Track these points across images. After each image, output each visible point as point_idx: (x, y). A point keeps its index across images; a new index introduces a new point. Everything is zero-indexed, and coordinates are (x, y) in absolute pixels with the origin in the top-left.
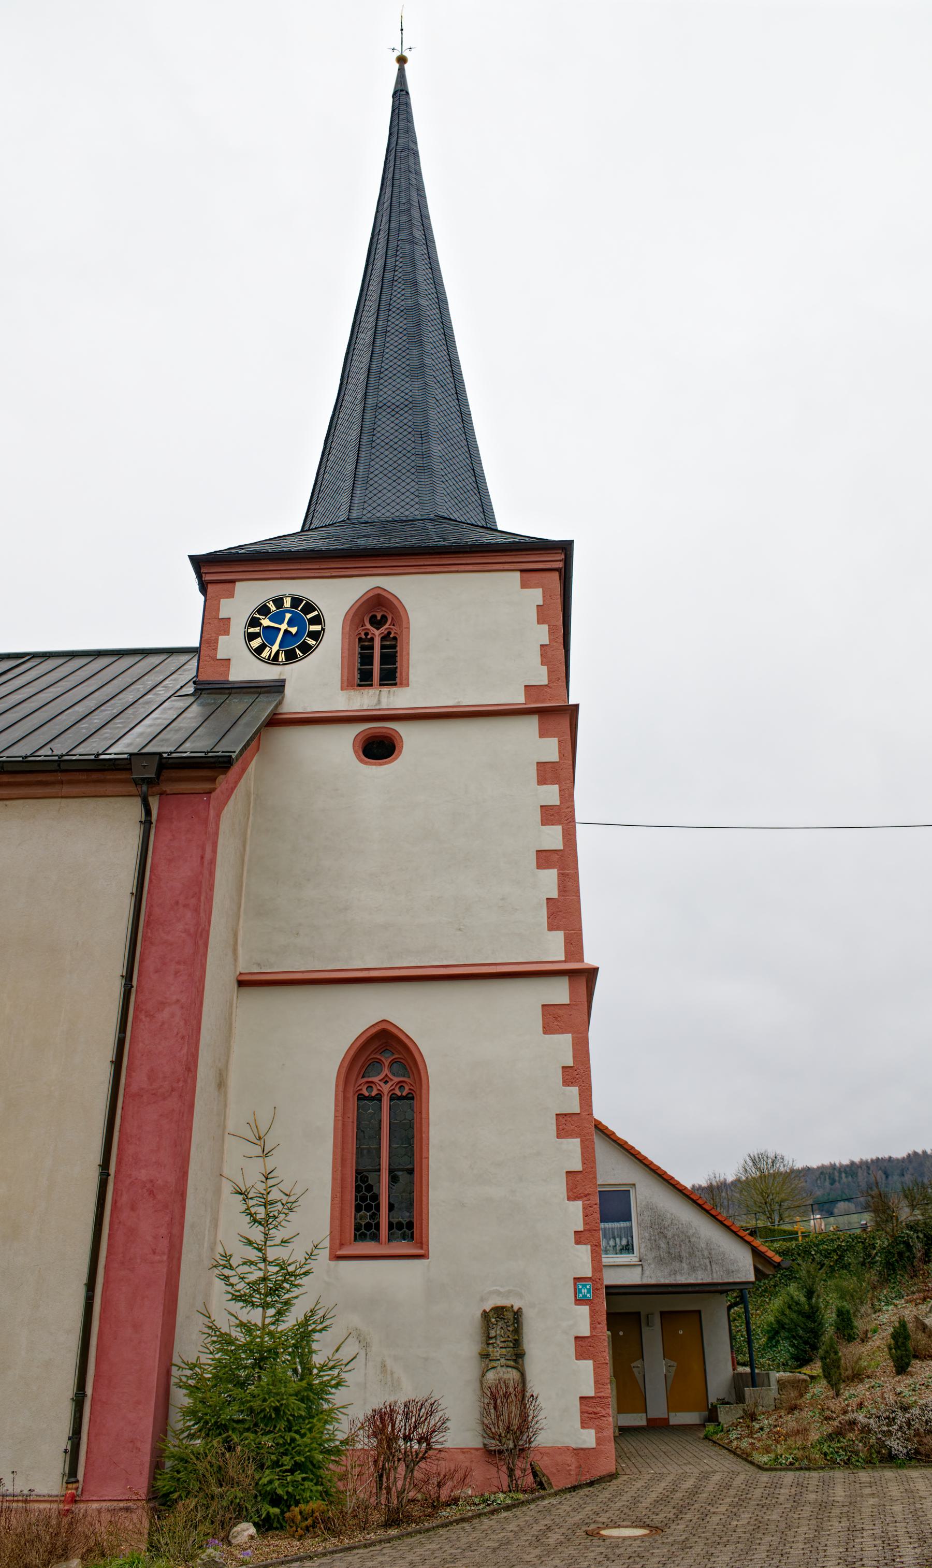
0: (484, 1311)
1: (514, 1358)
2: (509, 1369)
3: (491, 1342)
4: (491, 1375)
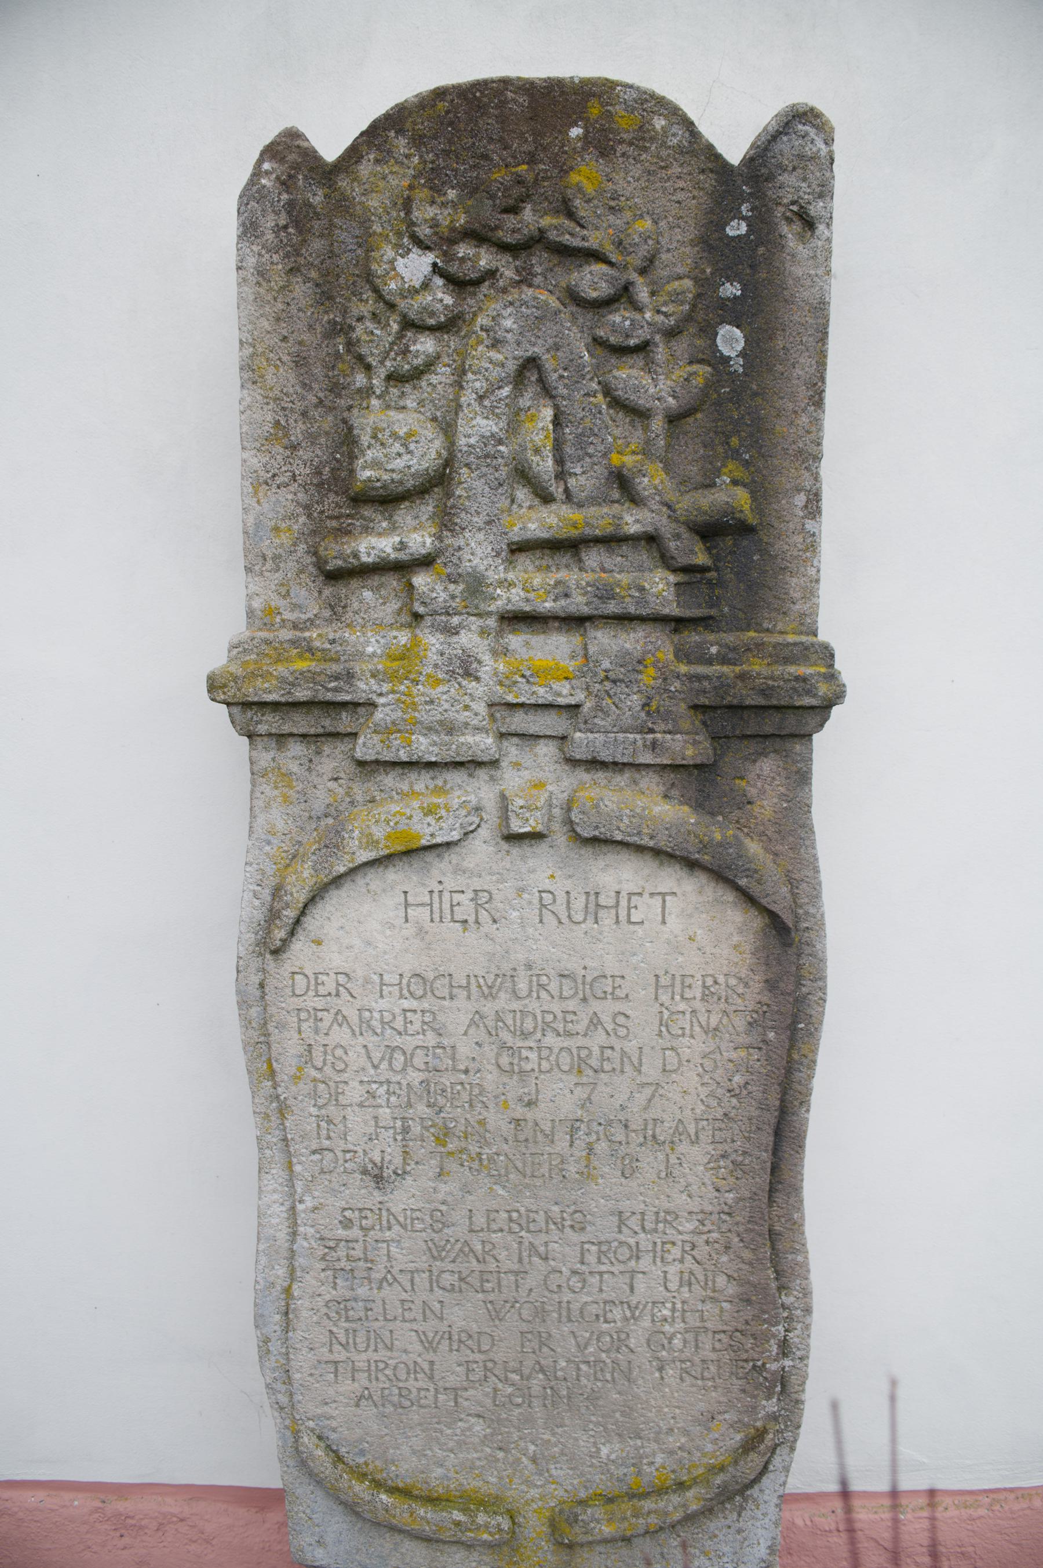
0: (288, 153)
1: (686, 746)
2: (619, 875)
3: (376, 545)
4: (367, 931)
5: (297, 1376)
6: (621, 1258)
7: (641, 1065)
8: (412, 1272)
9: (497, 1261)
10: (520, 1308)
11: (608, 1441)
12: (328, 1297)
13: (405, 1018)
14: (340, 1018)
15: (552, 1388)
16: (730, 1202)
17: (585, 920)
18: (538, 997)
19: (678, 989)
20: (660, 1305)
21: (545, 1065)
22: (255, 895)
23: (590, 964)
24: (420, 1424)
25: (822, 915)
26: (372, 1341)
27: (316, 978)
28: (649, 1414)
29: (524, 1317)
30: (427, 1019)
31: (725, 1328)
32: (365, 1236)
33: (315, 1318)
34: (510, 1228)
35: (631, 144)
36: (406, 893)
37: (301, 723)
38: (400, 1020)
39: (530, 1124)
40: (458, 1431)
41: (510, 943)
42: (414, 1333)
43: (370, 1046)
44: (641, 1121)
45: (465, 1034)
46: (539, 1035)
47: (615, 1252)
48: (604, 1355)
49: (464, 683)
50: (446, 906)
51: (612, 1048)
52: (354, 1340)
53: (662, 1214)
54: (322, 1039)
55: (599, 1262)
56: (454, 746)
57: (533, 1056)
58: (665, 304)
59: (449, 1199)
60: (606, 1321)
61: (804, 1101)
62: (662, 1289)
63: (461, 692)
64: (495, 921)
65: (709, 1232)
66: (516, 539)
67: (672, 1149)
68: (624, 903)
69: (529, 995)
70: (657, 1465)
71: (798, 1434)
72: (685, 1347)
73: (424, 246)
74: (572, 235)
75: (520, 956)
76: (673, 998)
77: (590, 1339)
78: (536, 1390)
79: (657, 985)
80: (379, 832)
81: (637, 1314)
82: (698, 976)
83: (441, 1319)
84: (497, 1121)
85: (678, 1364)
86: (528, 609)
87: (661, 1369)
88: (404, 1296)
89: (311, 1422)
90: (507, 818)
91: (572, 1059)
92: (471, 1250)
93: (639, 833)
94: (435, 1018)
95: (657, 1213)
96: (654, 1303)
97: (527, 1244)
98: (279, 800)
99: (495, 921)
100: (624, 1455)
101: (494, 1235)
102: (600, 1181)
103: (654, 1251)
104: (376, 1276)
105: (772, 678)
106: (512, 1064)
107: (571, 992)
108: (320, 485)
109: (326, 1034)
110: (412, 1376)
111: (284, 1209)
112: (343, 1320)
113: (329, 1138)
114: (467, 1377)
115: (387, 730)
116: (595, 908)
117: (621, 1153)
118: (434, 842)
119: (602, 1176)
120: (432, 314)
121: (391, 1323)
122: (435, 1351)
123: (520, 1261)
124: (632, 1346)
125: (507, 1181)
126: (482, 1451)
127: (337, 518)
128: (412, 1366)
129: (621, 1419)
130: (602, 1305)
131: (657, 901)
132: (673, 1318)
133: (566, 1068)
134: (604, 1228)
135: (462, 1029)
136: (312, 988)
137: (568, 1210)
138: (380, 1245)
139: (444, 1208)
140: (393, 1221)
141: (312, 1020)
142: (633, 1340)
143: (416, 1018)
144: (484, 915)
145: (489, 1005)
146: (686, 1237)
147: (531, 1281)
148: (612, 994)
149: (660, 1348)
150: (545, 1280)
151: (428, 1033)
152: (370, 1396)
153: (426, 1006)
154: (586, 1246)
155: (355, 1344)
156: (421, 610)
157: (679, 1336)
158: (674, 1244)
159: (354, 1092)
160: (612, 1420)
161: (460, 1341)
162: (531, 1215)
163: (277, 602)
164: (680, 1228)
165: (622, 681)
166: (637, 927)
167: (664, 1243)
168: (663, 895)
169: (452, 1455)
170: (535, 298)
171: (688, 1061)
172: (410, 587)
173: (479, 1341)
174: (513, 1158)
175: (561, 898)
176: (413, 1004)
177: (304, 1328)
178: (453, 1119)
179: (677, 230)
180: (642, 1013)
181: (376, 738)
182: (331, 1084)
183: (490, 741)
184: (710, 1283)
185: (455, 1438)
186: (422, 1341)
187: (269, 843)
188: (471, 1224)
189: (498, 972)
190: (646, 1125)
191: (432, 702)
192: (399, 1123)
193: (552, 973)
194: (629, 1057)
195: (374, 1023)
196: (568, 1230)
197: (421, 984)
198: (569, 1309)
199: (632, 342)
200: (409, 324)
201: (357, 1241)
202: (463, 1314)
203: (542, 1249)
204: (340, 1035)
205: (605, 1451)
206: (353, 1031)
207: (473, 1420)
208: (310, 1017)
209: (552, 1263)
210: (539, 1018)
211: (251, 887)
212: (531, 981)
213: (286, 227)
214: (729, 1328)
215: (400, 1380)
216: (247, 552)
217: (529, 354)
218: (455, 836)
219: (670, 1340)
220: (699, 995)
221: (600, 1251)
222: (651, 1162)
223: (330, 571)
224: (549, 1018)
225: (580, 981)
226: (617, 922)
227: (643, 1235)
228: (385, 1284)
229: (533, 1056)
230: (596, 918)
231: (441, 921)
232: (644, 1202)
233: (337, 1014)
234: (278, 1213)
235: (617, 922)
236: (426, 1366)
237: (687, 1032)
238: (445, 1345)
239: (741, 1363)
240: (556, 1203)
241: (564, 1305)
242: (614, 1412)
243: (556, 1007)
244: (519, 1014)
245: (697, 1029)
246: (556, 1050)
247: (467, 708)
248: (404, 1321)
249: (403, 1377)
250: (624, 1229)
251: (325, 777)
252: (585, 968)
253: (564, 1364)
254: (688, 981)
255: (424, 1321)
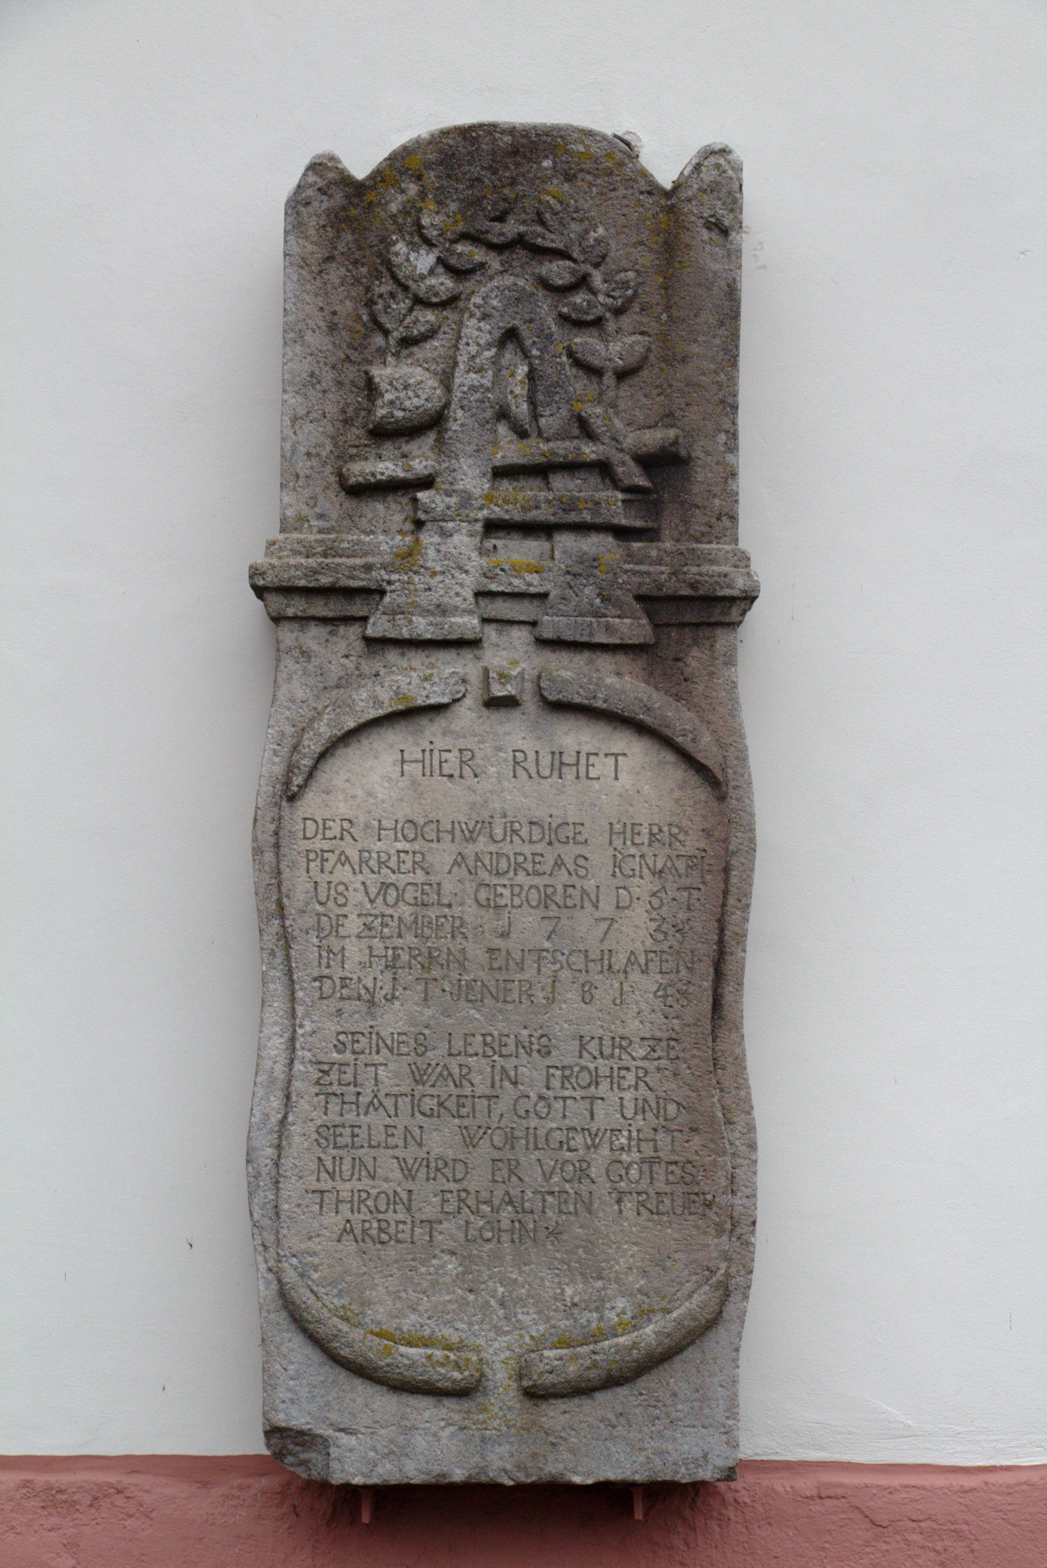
3: (386, 466)
4: (372, 780)
5: (286, 1207)
6: (582, 1083)
7: (598, 901)
8: (396, 1096)
9: (472, 1085)
10: (492, 1134)
11: (572, 1281)
12: (319, 1122)
13: (399, 857)
14: (343, 858)
15: (520, 1222)
16: (677, 1028)
17: (551, 774)
18: (512, 841)
19: (629, 835)
20: (617, 1133)
21: (517, 901)
22: (275, 753)
23: (555, 812)
24: (396, 1262)
25: (749, 775)
26: (357, 1168)
27: (324, 824)
28: (610, 1251)
29: (496, 1143)
30: (417, 859)
31: (677, 1158)
32: (356, 1059)
33: (306, 1144)
34: (484, 1052)
35: (589, 173)
36: (402, 751)
37: (320, 608)
38: (394, 858)
39: (504, 954)
40: (432, 1269)
41: (489, 794)
42: (395, 1161)
43: (368, 883)
44: (598, 952)
45: (450, 872)
46: (511, 874)
47: (577, 1077)
48: (567, 1186)
49: (457, 575)
50: (436, 762)
51: (574, 886)
52: (340, 1168)
53: (618, 1039)
54: (326, 877)
55: (563, 1087)
56: (446, 626)
57: (507, 892)
58: (613, 290)
59: (432, 1022)
60: (569, 1150)
61: (741, 937)
62: (618, 1116)
63: (453, 582)
64: (476, 776)
65: (659, 1058)
66: (498, 464)
67: (626, 978)
68: (583, 761)
69: (504, 839)
70: (618, 1310)
71: (751, 1280)
72: (641, 1178)
73: (429, 243)
74: (544, 238)
75: (497, 805)
76: (624, 844)
77: (554, 1168)
78: (505, 1224)
79: (611, 831)
80: (385, 695)
81: (597, 1141)
82: (646, 825)
83: (420, 1145)
84: (476, 952)
85: (635, 1195)
86: (507, 517)
87: (619, 1201)
88: (388, 1121)
89: (294, 1259)
90: (489, 684)
91: (540, 896)
92: (450, 1074)
93: (594, 697)
94: (423, 858)
95: (613, 1038)
96: (612, 1130)
97: (499, 1067)
98: (300, 673)
99: (476, 776)
100: (587, 1298)
101: (470, 1059)
102: (564, 1006)
103: (611, 1077)
104: (364, 1100)
105: (700, 574)
106: (488, 899)
107: (540, 837)
108: (345, 421)
109: (331, 872)
110: (392, 1207)
111: (283, 1041)
112: (331, 1146)
113: (328, 966)
114: (442, 1208)
115: (393, 612)
116: (559, 765)
117: (582, 981)
118: (428, 702)
119: (565, 1001)
120: (436, 294)
121: (373, 1150)
122: (413, 1179)
123: (493, 1086)
124: (593, 1175)
125: (483, 1006)
126: (454, 1292)
127: (357, 447)
128: (391, 1197)
129: (584, 1256)
130: (565, 1132)
131: (611, 761)
132: (629, 1146)
133: (534, 903)
134: (566, 1053)
135: (447, 868)
136: (321, 831)
137: (535, 1034)
138: (369, 1068)
139: (427, 1032)
140: (381, 1044)
141: (319, 860)
142: (593, 1170)
143: (408, 859)
144: (467, 771)
145: (470, 847)
146: (640, 1063)
147: (502, 1106)
148: (574, 838)
149: (618, 1178)
150: (515, 1105)
151: (417, 871)
152: (352, 1230)
153: (416, 847)
154: (552, 1071)
155: (341, 1172)
156: (422, 516)
157: (635, 1166)
158: (628, 1069)
159: (353, 925)
160: (575, 1258)
161: (437, 1169)
162: (504, 1039)
163: (306, 511)
164: (634, 1054)
165: (580, 575)
166: (594, 782)
167: (619, 1068)
168: (616, 755)
169: (426, 1299)
170: (516, 284)
171: (638, 899)
172: (415, 500)
173: (454, 1169)
174: (488, 984)
175: (531, 756)
176: (407, 846)
177: (295, 1154)
178: (437, 949)
179: (623, 236)
180: (600, 858)
181: (385, 617)
182: (333, 916)
183: (476, 621)
184: (662, 1111)
185: (429, 1277)
186: (402, 1169)
187: (289, 709)
188: (450, 1048)
189: (479, 819)
190: (602, 955)
191: (430, 589)
192: (390, 952)
193: (523, 821)
194: (588, 895)
195: (372, 863)
196: (535, 1054)
197: (415, 829)
198: (535, 1135)
199: (589, 318)
200: (420, 302)
201: (348, 1065)
202: (441, 1140)
203: (512, 1073)
204: (343, 873)
205: (569, 1291)
206: (353, 869)
207: (447, 1257)
208: (317, 856)
209: (521, 1087)
210: (512, 859)
211: (272, 746)
212: (505, 828)
213: (324, 226)
214: (681, 1158)
215: (380, 1212)
216: (283, 472)
217: (509, 326)
218: (445, 700)
219: (627, 1169)
220: (646, 841)
221: (564, 1077)
222: (606, 988)
223: (352, 487)
224: (521, 859)
225: (546, 827)
226: (578, 777)
227: (600, 1060)
228: (371, 1109)
229: (507, 892)
230: (560, 774)
231: (431, 775)
232: (602, 1027)
233: (341, 854)
234: (276, 1046)
235: (578, 777)
236: (404, 1196)
237: (637, 873)
238: (422, 1174)
239: (693, 1197)
240: (525, 1027)
241: (531, 1131)
242: (578, 1247)
243: (527, 850)
244: (495, 856)
245: (645, 870)
246: (526, 888)
247: (457, 594)
248: (387, 1147)
249: (383, 1208)
250: (585, 1053)
251: (339, 655)
252: (551, 816)
253: (531, 1195)
254: (637, 829)
255: (405, 1148)
